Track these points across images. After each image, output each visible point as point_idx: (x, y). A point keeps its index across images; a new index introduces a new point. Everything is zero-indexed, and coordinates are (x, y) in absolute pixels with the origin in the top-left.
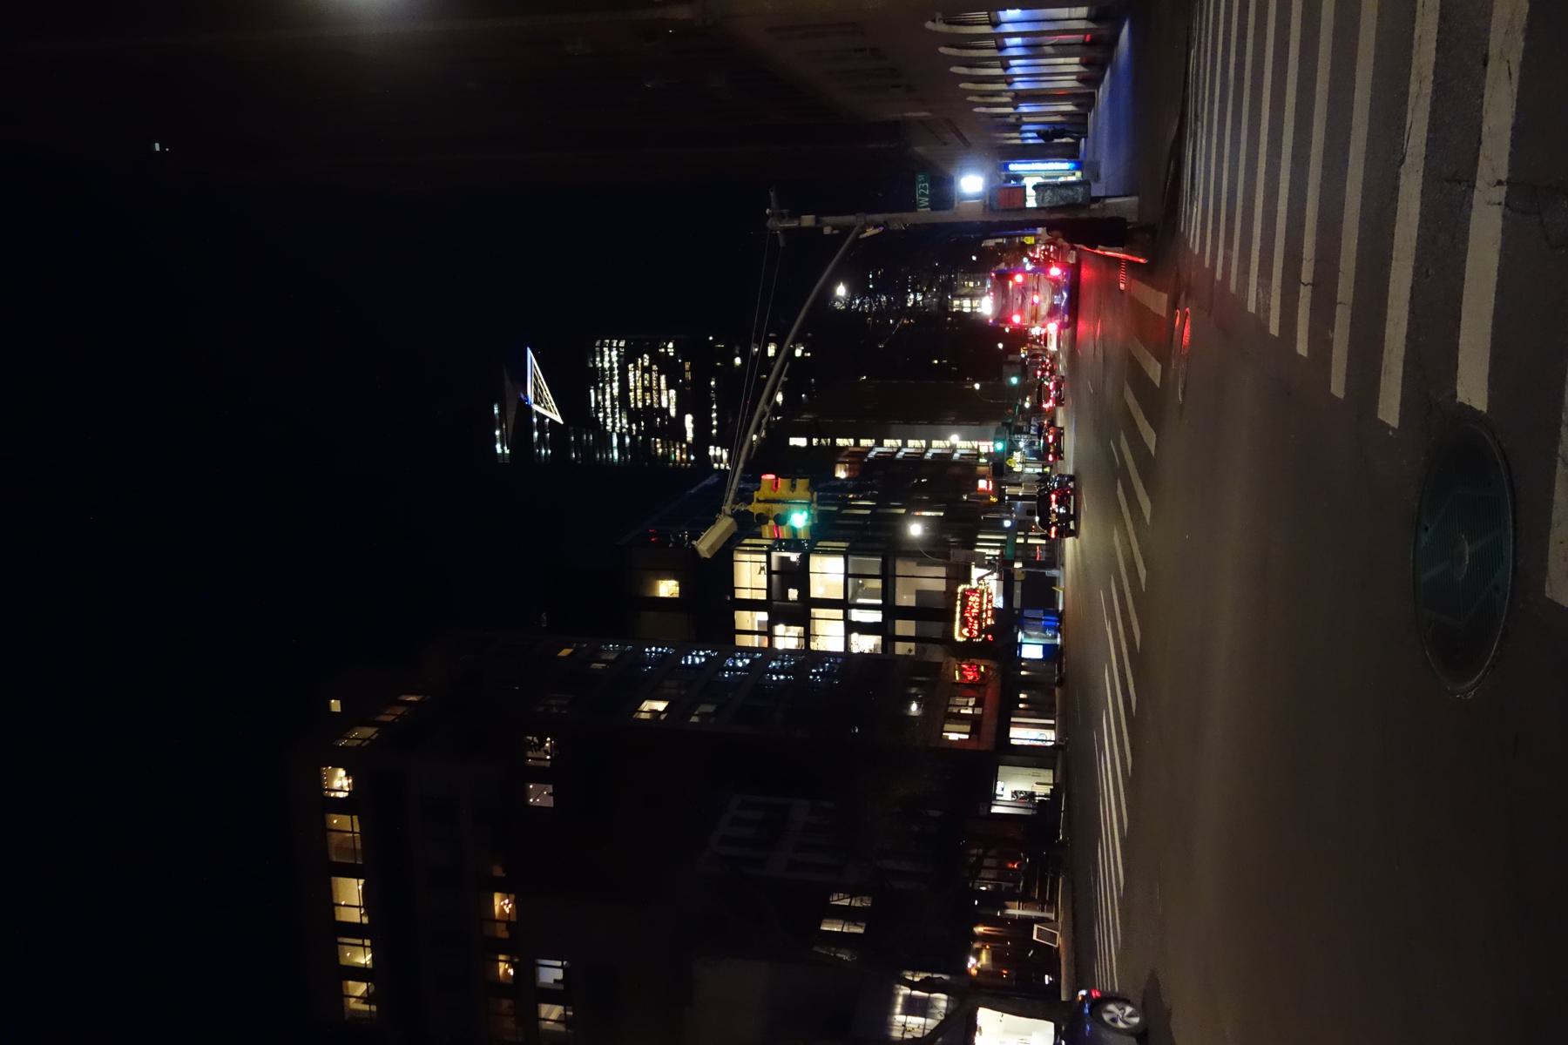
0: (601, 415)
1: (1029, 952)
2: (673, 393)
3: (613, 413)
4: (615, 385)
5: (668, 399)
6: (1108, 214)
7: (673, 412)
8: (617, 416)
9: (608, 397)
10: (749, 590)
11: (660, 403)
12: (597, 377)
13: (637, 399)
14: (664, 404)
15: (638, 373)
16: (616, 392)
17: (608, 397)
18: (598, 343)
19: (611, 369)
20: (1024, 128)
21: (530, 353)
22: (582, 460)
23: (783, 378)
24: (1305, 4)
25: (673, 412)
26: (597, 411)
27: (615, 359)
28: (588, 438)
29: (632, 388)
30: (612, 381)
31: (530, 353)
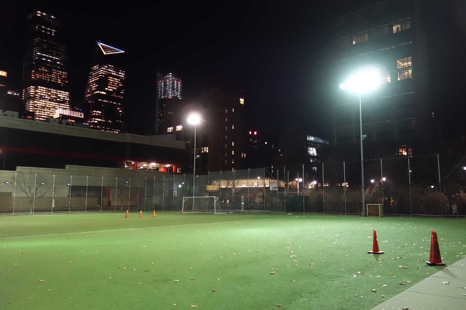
9: (112, 71)
12: (117, 70)
16: (112, 73)
17: (112, 71)
19: (119, 74)
21: (124, 52)
31: (124, 52)
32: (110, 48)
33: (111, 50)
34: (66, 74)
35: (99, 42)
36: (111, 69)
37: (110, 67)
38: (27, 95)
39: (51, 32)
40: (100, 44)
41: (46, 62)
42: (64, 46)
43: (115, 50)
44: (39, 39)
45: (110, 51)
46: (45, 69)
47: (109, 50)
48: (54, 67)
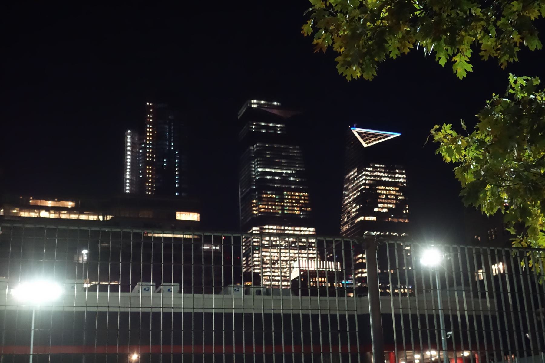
0: (371, 169)
1: (352, 5)
2: (385, 210)
3: (371, 176)
4: (387, 179)
5: (382, 208)
6: (209, 245)
7: (376, 210)
8: (372, 178)
9: (382, 174)
10: (194, 299)
11: (381, 203)
12: (390, 170)
13: (381, 190)
14: (380, 205)
15: (394, 193)
16: (383, 179)
17: (382, 174)
18: (404, 171)
19: (395, 178)
20: (321, 262)
22: (533, 155)
23: (541, 309)
24: (476, 362)
25: (376, 210)
26: (372, 167)
27: (400, 180)
28: (268, 154)
29: (387, 188)
30: (390, 178)
32: (373, 134)
33: (376, 137)
34: (306, 196)
35: (353, 127)
36: (380, 172)
37: (377, 168)
38: (248, 244)
39: (275, 128)
40: (355, 131)
41: (273, 181)
42: (297, 147)
43: (381, 135)
44: (258, 145)
45: (374, 139)
46: (272, 194)
47: (372, 137)
48: (285, 187)
